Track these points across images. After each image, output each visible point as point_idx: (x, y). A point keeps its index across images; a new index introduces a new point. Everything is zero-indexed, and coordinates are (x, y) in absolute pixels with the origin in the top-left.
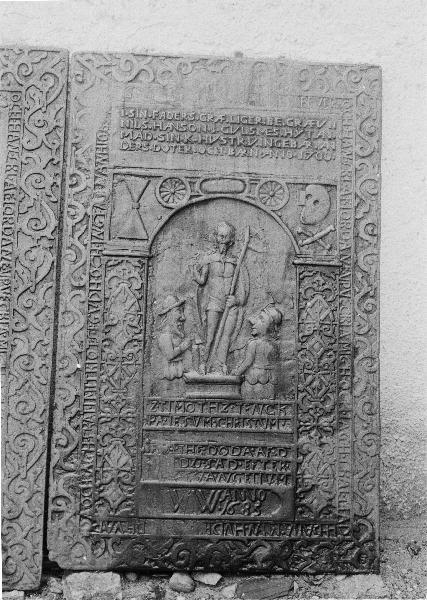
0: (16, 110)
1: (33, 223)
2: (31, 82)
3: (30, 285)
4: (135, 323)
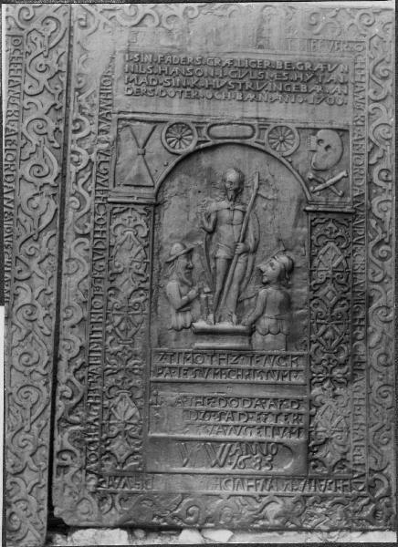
1: (36, 169)
4: (141, 271)
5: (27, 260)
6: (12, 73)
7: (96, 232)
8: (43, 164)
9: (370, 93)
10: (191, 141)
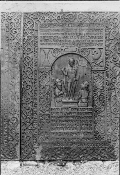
0: (107, 29)
1: (114, 59)
2: (111, 21)
3: (114, 76)
5: (113, 84)
6: (106, 34)
7: (34, 78)
8: (116, 58)
9: (110, 38)
10: (60, 53)
